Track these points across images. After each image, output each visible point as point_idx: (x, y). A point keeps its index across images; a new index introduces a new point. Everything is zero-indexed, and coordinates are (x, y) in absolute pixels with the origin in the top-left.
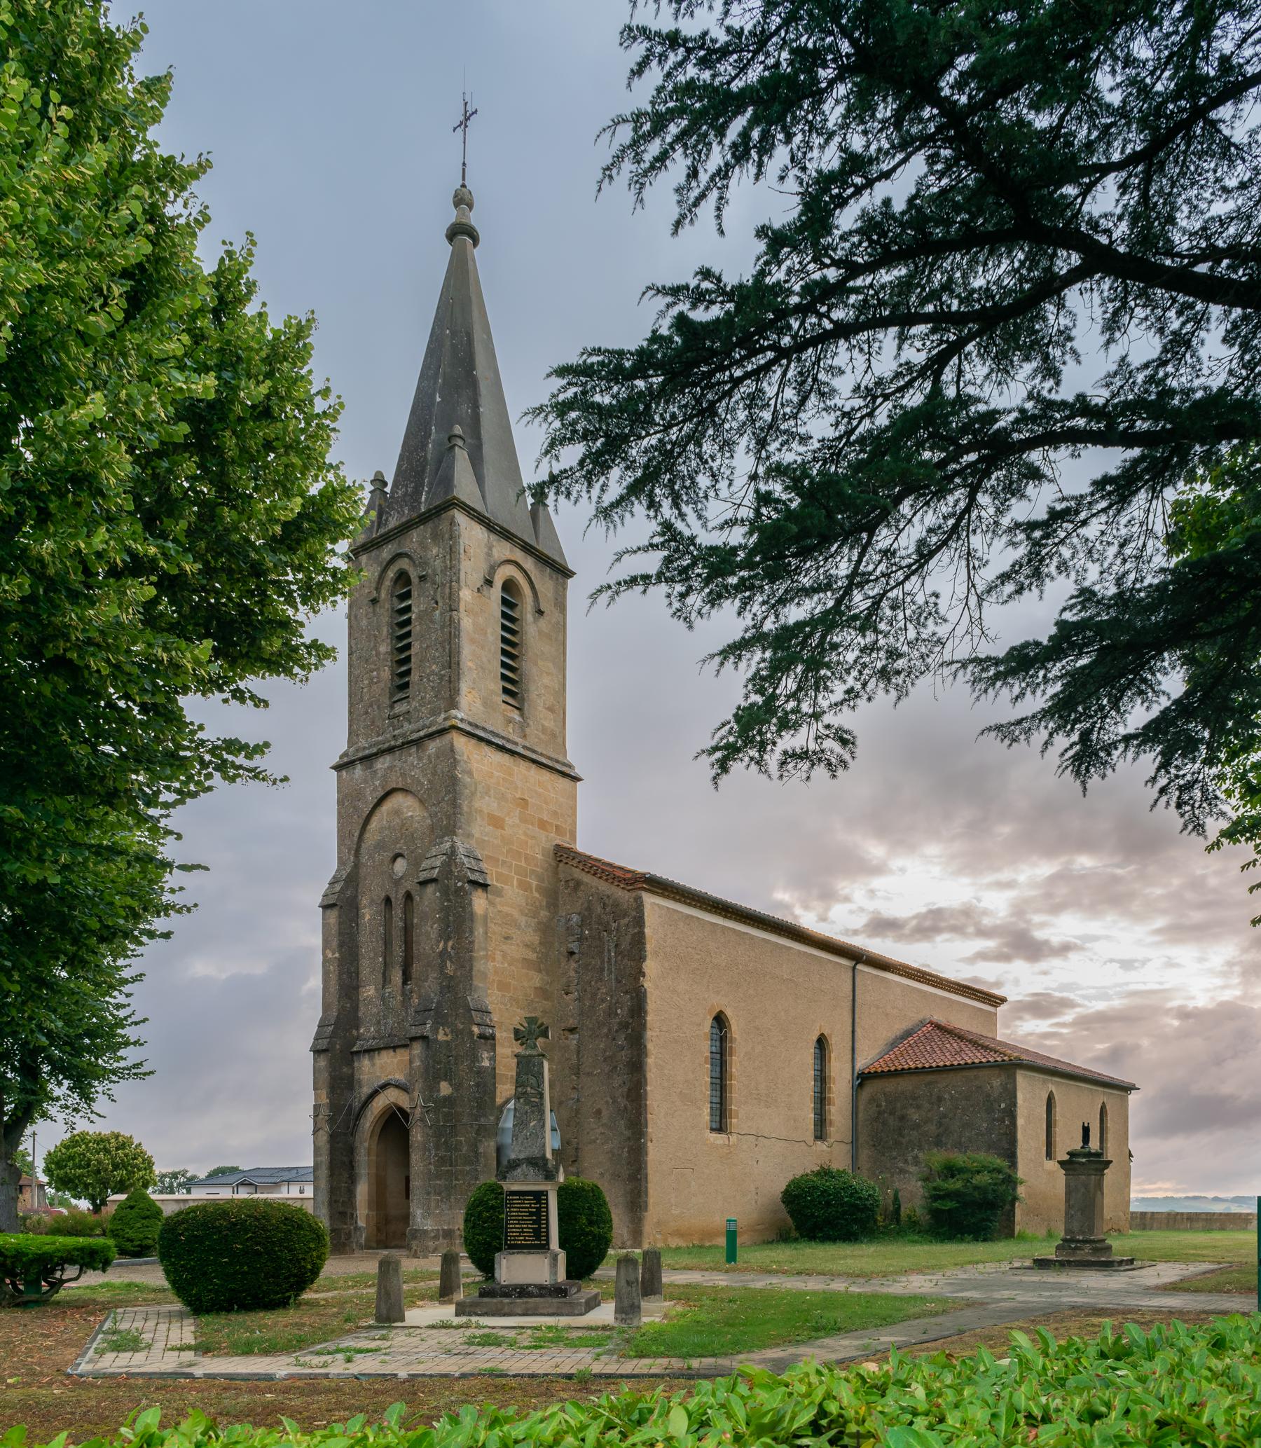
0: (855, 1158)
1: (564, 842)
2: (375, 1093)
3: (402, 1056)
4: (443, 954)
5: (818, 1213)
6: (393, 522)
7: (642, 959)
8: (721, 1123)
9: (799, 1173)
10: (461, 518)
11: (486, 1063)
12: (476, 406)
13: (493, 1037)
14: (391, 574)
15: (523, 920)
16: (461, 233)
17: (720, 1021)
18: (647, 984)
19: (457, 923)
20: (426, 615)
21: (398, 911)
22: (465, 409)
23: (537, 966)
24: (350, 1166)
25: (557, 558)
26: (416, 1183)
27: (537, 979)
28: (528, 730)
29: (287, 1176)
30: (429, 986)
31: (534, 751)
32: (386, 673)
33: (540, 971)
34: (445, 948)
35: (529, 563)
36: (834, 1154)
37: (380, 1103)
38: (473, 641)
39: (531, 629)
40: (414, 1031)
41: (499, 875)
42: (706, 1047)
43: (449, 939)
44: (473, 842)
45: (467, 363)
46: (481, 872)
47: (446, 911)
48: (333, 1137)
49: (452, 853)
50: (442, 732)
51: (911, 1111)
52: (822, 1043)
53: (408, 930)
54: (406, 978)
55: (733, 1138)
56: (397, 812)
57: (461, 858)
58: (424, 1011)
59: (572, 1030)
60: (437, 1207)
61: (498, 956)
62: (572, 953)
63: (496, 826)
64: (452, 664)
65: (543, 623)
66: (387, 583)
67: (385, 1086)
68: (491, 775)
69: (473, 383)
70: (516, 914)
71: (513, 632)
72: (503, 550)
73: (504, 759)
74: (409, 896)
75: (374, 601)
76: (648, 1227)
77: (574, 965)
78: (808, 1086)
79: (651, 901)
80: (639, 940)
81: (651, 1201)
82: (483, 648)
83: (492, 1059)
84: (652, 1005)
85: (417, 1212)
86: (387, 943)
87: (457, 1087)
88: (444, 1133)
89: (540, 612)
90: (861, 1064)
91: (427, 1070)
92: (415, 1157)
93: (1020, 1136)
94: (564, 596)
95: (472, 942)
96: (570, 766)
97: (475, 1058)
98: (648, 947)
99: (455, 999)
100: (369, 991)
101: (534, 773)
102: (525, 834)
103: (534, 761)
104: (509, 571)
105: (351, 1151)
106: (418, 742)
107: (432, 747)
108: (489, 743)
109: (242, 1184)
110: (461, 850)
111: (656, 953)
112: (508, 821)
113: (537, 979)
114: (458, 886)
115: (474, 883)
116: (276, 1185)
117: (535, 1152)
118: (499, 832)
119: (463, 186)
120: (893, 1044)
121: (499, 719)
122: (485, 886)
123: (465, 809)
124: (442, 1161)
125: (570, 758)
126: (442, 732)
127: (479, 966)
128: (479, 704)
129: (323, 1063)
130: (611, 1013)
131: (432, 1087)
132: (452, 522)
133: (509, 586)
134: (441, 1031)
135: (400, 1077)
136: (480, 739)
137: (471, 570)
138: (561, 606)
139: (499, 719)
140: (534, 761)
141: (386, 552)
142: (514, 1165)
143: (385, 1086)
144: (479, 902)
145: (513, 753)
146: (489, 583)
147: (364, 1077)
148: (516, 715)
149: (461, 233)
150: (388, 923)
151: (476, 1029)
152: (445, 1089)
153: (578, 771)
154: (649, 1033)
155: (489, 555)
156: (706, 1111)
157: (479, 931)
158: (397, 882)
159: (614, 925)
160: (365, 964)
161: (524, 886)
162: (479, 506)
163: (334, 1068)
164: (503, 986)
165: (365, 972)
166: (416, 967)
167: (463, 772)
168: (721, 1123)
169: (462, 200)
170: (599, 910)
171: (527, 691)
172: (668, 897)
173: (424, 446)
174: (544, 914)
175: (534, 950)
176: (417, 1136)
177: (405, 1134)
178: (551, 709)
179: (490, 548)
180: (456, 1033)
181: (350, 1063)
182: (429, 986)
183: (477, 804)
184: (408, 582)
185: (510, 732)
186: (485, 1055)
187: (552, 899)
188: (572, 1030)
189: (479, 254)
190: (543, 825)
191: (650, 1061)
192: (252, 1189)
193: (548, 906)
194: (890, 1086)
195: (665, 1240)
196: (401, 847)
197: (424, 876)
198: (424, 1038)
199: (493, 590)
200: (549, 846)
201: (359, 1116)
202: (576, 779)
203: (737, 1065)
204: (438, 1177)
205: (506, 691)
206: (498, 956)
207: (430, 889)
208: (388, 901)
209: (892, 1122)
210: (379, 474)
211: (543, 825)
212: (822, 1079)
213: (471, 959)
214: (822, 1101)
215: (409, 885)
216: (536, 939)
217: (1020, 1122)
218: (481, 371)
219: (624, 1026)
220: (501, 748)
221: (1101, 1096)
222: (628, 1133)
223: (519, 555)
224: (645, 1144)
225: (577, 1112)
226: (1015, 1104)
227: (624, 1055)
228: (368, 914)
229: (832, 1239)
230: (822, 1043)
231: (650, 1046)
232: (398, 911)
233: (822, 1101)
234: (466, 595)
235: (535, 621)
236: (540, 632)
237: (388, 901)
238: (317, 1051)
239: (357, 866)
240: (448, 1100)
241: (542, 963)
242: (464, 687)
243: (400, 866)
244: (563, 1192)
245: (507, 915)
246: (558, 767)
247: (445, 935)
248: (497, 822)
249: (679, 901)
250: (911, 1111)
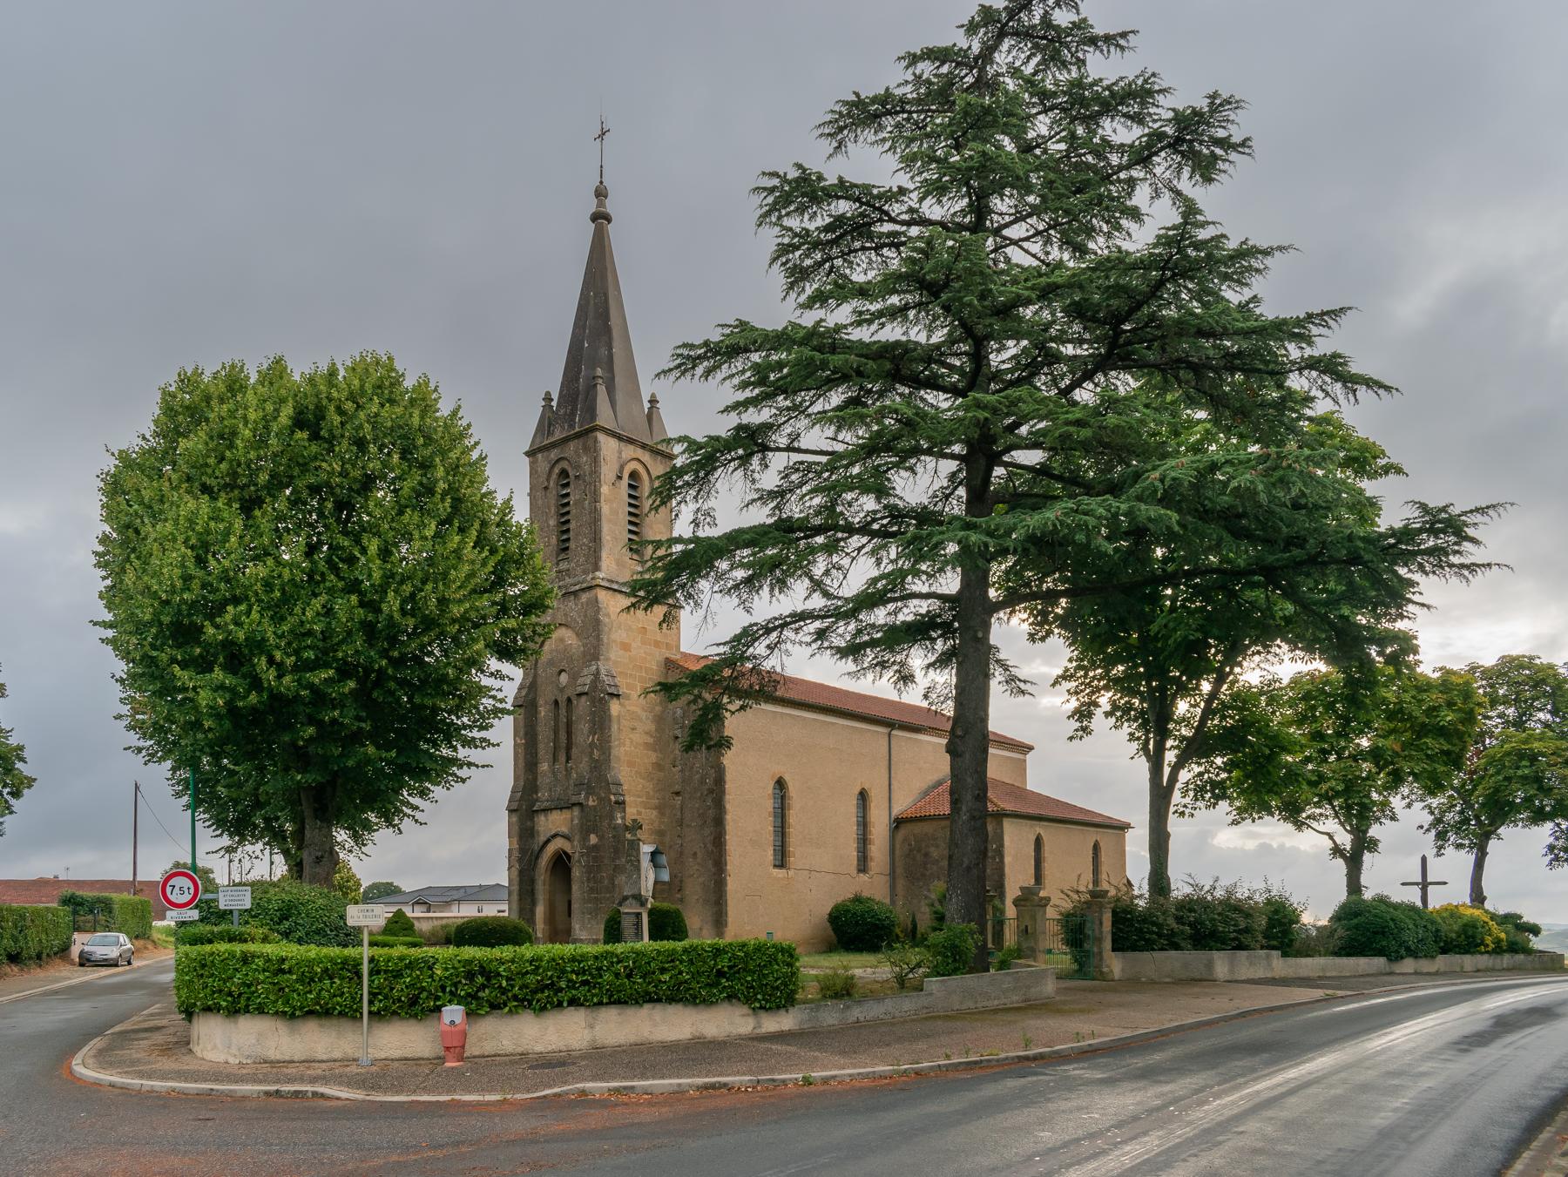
0: (893, 887)
2: (548, 841)
3: (566, 814)
4: (592, 745)
5: (854, 929)
6: (558, 435)
8: (782, 860)
9: (840, 900)
10: (601, 437)
12: (610, 349)
13: (624, 802)
14: (556, 471)
15: (644, 715)
16: (600, 217)
17: (780, 784)
19: (601, 722)
20: (579, 503)
21: (563, 711)
22: (603, 352)
24: (532, 893)
26: (575, 906)
29: (456, 895)
30: (582, 767)
32: (554, 540)
36: (874, 887)
37: (551, 848)
40: (574, 799)
42: (770, 805)
45: (604, 316)
47: (593, 714)
48: (521, 872)
49: (597, 673)
50: (590, 588)
51: (932, 849)
52: (863, 796)
53: (569, 725)
54: (568, 758)
55: (791, 873)
56: (562, 640)
57: (603, 676)
58: (579, 784)
59: (677, 794)
61: (628, 742)
64: (596, 539)
66: (554, 476)
67: (554, 836)
69: (608, 330)
70: (639, 711)
71: (635, 498)
72: (630, 451)
74: (569, 700)
75: (546, 488)
78: (852, 829)
81: (730, 920)
84: (728, 777)
85: (576, 926)
86: (556, 732)
87: (601, 838)
88: (592, 871)
90: (896, 811)
91: (582, 825)
92: (575, 887)
93: (1007, 870)
97: (612, 818)
99: (600, 779)
100: (544, 767)
105: (533, 881)
106: (575, 593)
107: (584, 597)
109: (417, 903)
110: (603, 671)
112: (634, 645)
114: (601, 696)
115: (612, 695)
116: (447, 904)
117: (635, 891)
120: (926, 793)
122: (618, 696)
124: (592, 890)
126: (590, 588)
127: (614, 752)
128: (614, 565)
129: (514, 819)
130: (702, 782)
131: (585, 838)
132: (596, 440)
135: (564, 830)
137: (608, 471)
141: (554, 454)
142: (625, 898)
143: (554, 836)
147: (541, 829)
149: (600, 217)
150: (556, 718)
152: (593, 839)
156: (771, 852)
157: (615, 727)
158: (562, 690)
160: (541, 746)
163: (521, 821)
164: (631, 764)
165: (541, 753)
166: (574, 751)
168: (782, 860)
169: (601, 193)
173: (577, 380)
176: (576, 873)
177: (568, 871)
179: (620, 452)
180: (600, 799)
181: (532, 820)
182: (582, 767)
183: (613, 636)
184: (567, 476)
188: (677, 794)
189: (611, 228)
191: (728, 817)
192: (424, 908)
194: (918, 828)
196: (564, 665)
197: (579, 689)
198: (580, 804)
200: (661, 659)
201: (537, 857)
203: (793, 817)
206: (628, 742)
207: (584, 698)
208: (556, 702)
209: (919, 857)
210: (548, 393)
212: (864, 824)
213: (610, 748)
214: (864, 841)
215: (570, 692)
216: (653, 727)
217: (1007, 860)
218: (614, 322)
219: (711, 791)
221: (1092, 835)
223: (640, 453)
225: (681, 853)
226: (1002, 845)
227: (711, 813)
228: (543, 712)
229: (860, 950)
230: (863, 796)
231: (728, 806)
232: (563, 711)
233: (864, 841)
234: (605, 490)
237: (556, 702)
238: (511, 811)
239: (535, 676)
240: (595, 846)
241: (657, 745)
242: (604, 555)
243: (564, 678)
244: (651, 913)
247: (593, 732)
248: (626, 647)
250: (932, 849)
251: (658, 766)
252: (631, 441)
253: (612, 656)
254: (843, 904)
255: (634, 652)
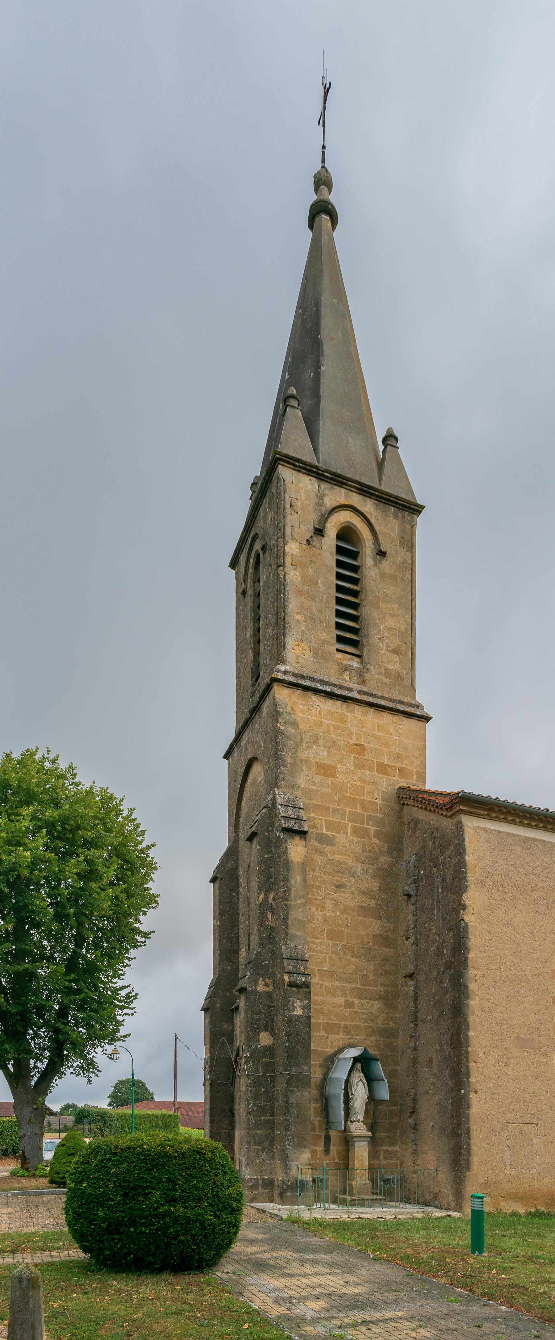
1: (412, 783)
7: (464, 889)
11: (299, 1012)
12: (317, 366)
13: (307, 985)
15: (358, 868)
18: (468, 917)
23: (375, 913)
25: (403, 495)
27: (375, 927)
28: (367, 676)
31: (372, 695)
33: (380, 918)
34: (266, 900)
35: (368, 506)
38: (300, 593)
39: (371, 571)
41: (329, 825)
43: (270, 890)
44: (298, 793)
46: (299, 819)
59: (411, 976)
60: (257, 1156)
62: (409, 896)
63: (325, 774)
65: (386, 565)
68: (320, 724)
70: (350, 861)
73: (338, 706)
76: (471, 1189)
77: (411, 908)
79: (472, 826)
80: (460, 869)
81: (475, 1159)
82: (313, 598)
83: (307, 1008)
84: (474, 941)
89: (382, 554)
94: (413, 534)
95: (289, 891)
96: (418, 706)
98: (470, 876)
101: (372, 717)
102: (362, 780)
103: (371, 705)
104: (345, 517)
105: (231, 1099)
108: (316, 691)
111: (482, 883)
112: (341, 768)
113: (375, 927)
118: (329, 781)
119: (323, 167)
121: (335, 667)
122: (302, 834)
123: (289, 760)
125: (419, 699)
127: (296, 914)
128: (308, 656)
130: (439, 954)
133: (346, 534)
134: (261, 982)
136: (306, 689)
138: (410, 545)
139: (335, 667)
140: (371, 705)
144: (296, 850)
145: (344, 699)
146: (319, 532)
148: (355, 663)
151: (286, 978)
152: (265, 1039)
153: (427, 711)
154: (471, 972)
155: (320, 504)
157: (296, 879)
159: (441, 859)
161: (360, 832)
162: (308, 457)
164: (334, 935)
167: (286, 723)
169: (322, 181)
170: (430, 845)
171: (367, 636)
172: (497, 819)
174: (384, 860)
175: (372, 897)
178: (396, 651)
179: (321, 497)
185: (347, 680)
186: (298, 1003)
187: (395, 844)
188: (411, 976)
190: (383, 769)
191: (473, 1003)
193: (390, 851)
195: (496, 1204)
199: (324, 540)
202: (427, 719)
204: (258, 1127)
205: (340, 639)
206: (329, 905)
211: (383, 769)
216: (375, 886)
220: (331, 695)
222: (451, 1083)
223: (356, 500)
224: (466, 1096)
231: (472, 986)
234: (292, 548)
235: (376, 563)
236: (383, 575)
238: (205, 1009)
240: (270, 1051)
242: (291, 641)
245: (339, 863)
246: (401, 708)
248: (327, 771)
249: (513, 822)
251: (384, 940)
252: (338, 480)
253: (302, 781)
254: (468, 1122)
255: (340, 779)
